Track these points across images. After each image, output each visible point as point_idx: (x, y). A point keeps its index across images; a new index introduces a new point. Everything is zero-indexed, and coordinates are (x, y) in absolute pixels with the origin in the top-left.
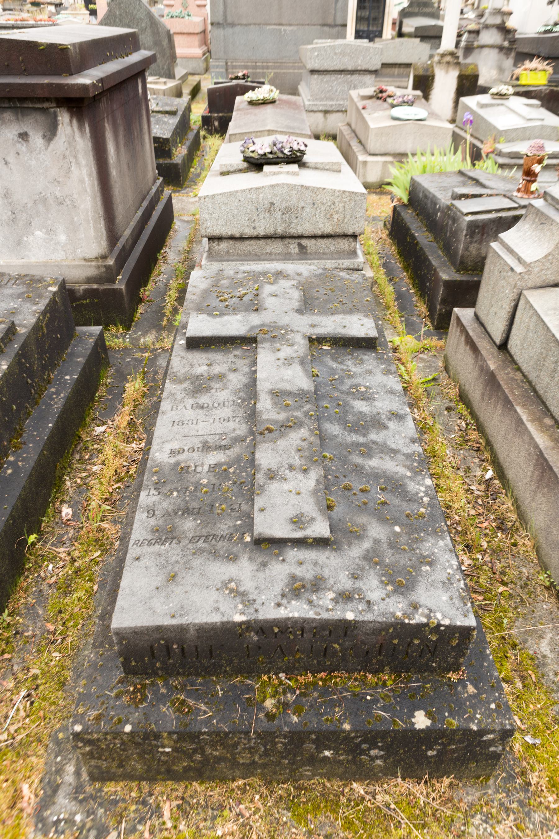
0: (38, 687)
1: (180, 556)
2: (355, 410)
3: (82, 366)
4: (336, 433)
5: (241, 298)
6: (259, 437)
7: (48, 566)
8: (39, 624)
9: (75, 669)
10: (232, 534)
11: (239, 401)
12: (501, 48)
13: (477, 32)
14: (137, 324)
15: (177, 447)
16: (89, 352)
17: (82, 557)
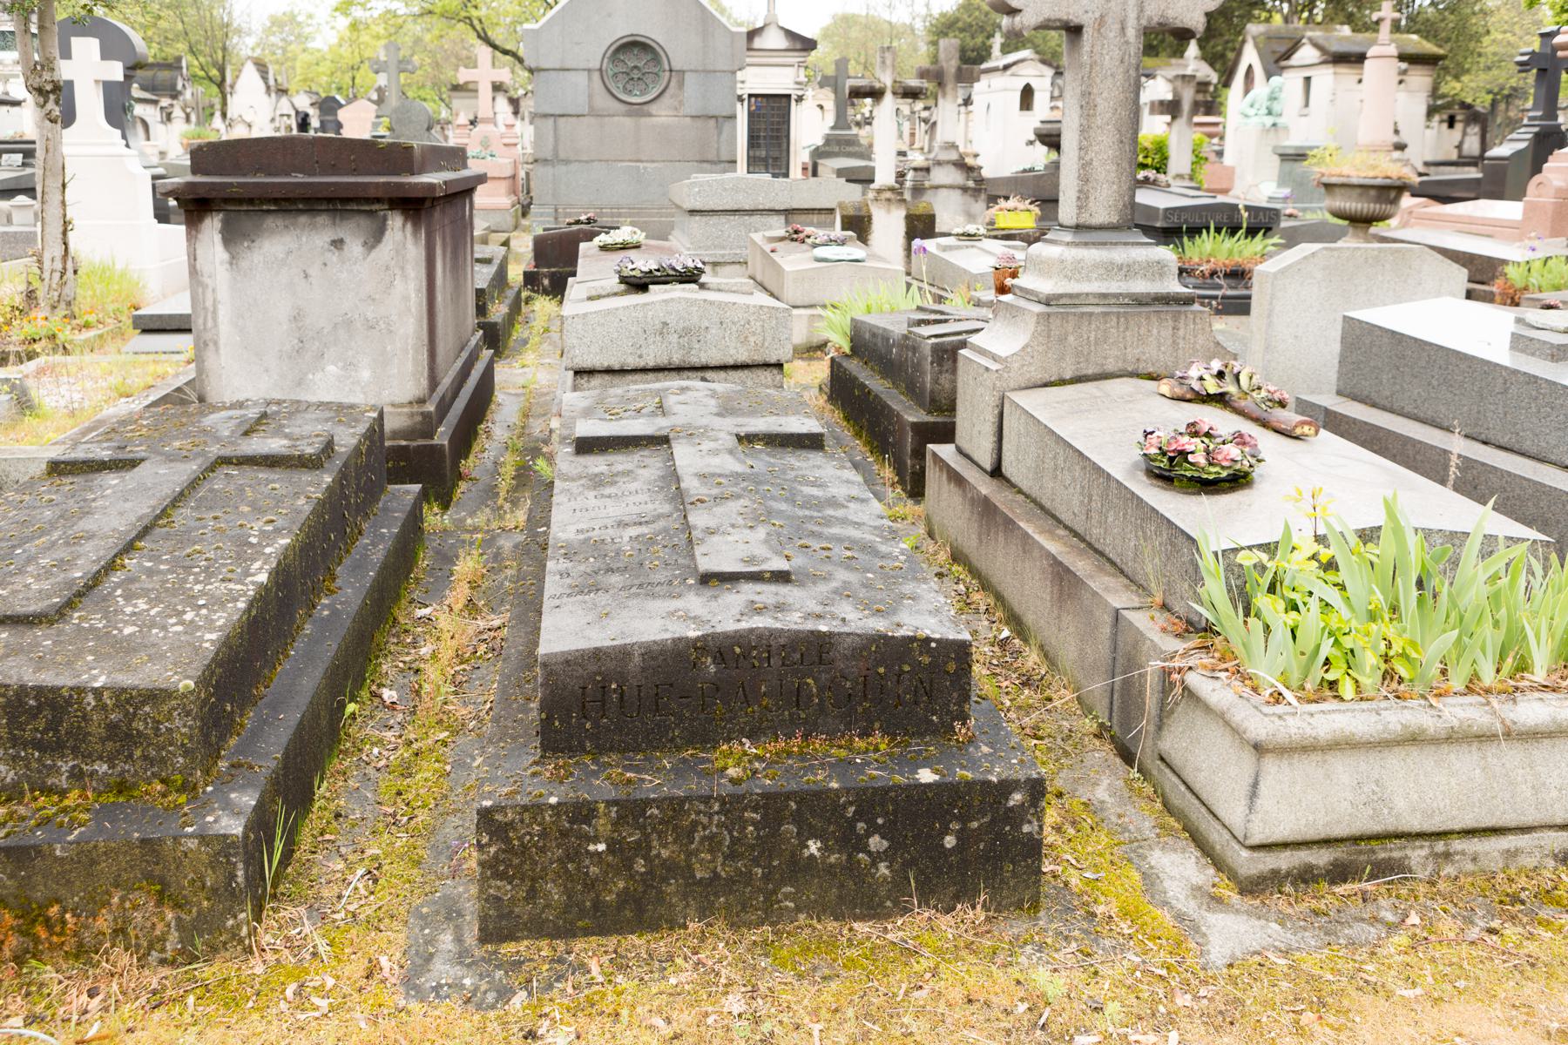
12: (965, 189)
13: (927, 170)
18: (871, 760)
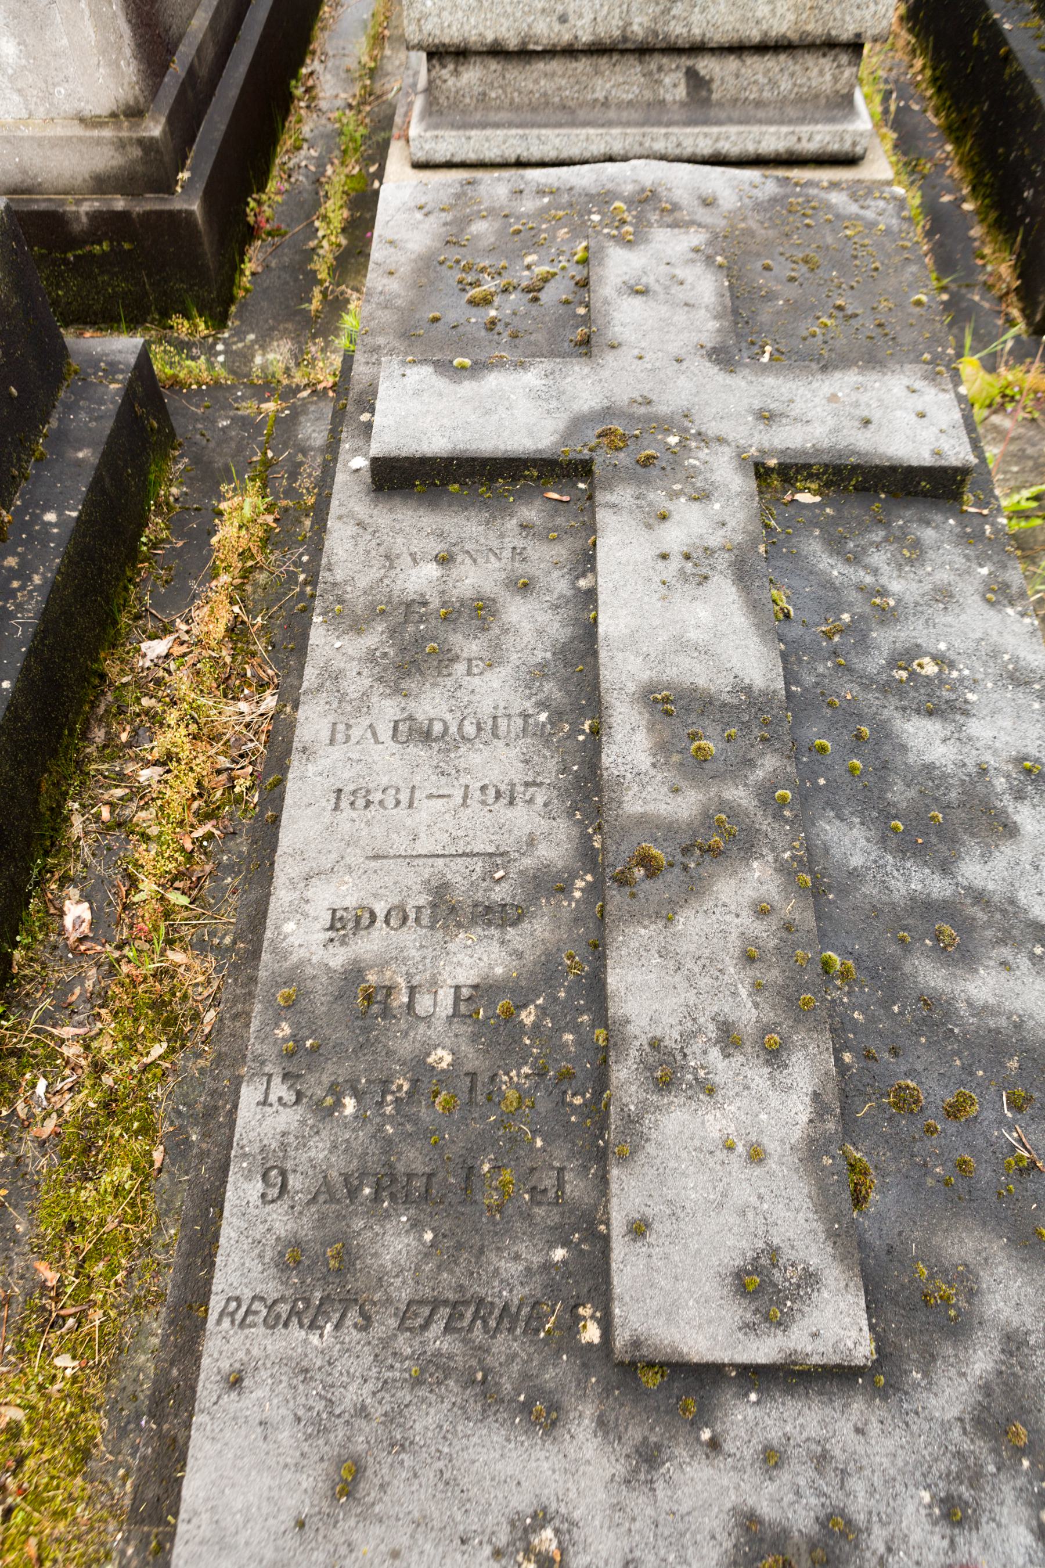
0: (20, 1461)
1: (370, 1386)
2: (911, 758)
3: (88, 476)
4: (857, 861)
5: (533, 291)
6: (616, 897)
7: (34, 1086)
8: (18, 1264)
9: (113, 1410)
10: (537, 1303)
11: (543, 717)
14: (243, 306)
15: (351, 902)
16: (109, 425)
17: (121, 1057)
18: (282, 1321)
